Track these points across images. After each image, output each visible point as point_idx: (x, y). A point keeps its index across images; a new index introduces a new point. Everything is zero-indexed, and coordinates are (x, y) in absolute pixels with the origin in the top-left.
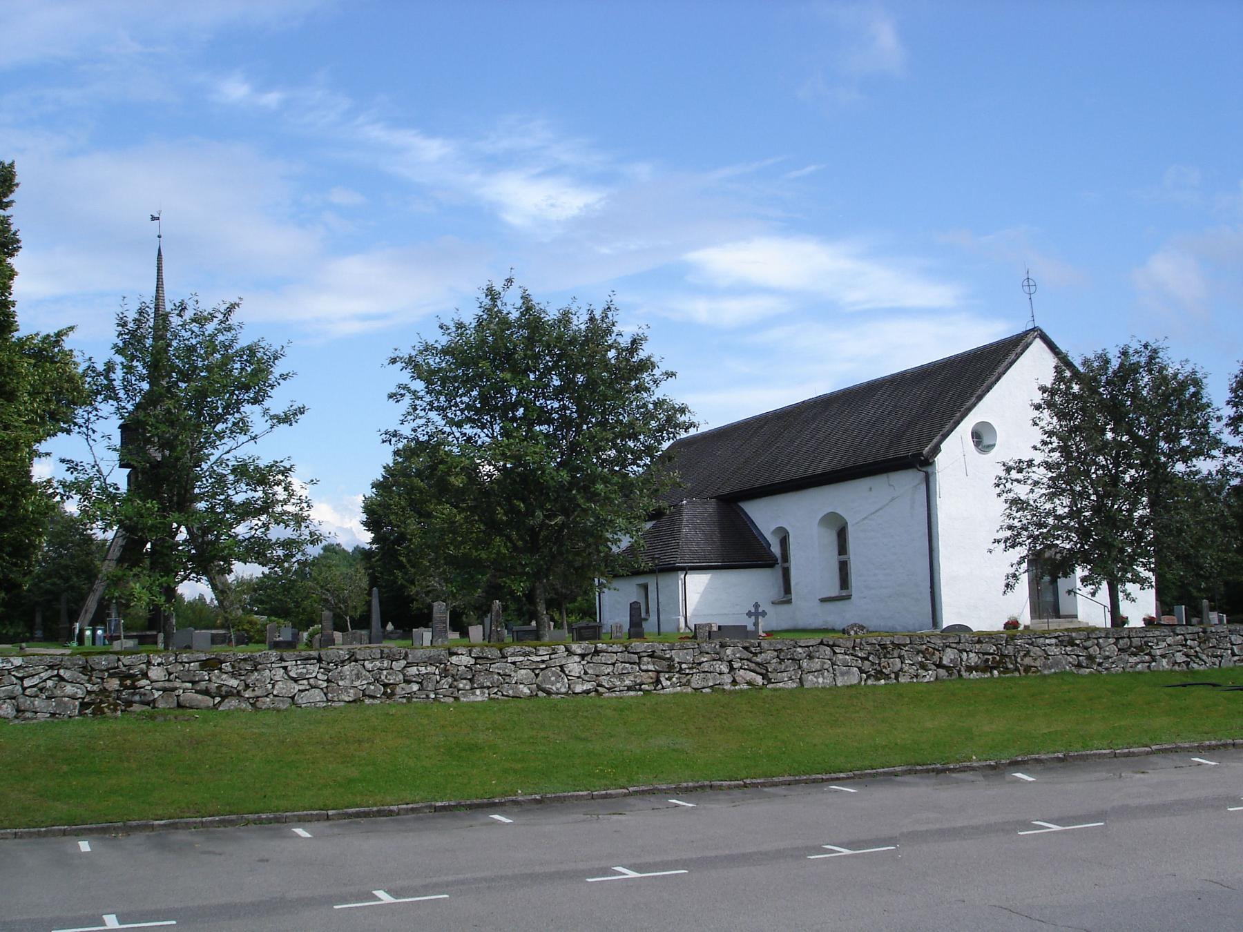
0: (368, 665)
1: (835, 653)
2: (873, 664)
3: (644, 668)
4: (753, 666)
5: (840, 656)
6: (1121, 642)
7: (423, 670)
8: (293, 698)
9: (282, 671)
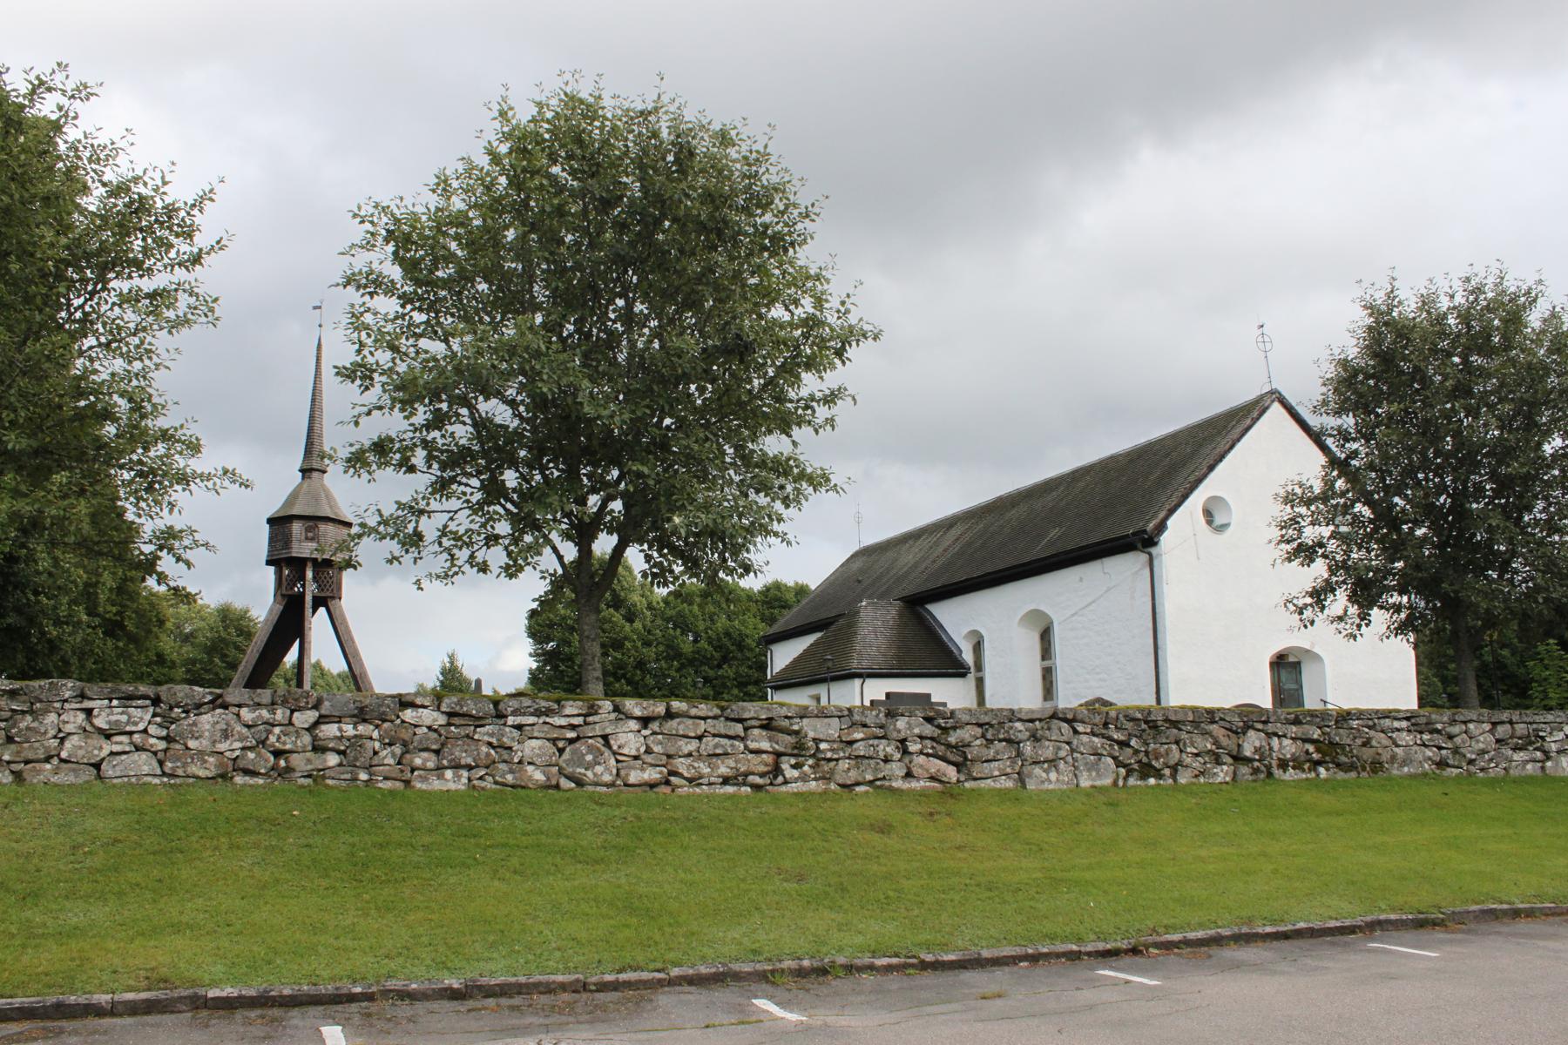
0: (246, 714)
1: (1076, 732)
2: (1136, 752)
3: (753, 745)
4: (941, 749)
5: (1085, 738)
6: (1500, 728)
7: (349, 730)
8: (97, 766)
9: (81, 716)
